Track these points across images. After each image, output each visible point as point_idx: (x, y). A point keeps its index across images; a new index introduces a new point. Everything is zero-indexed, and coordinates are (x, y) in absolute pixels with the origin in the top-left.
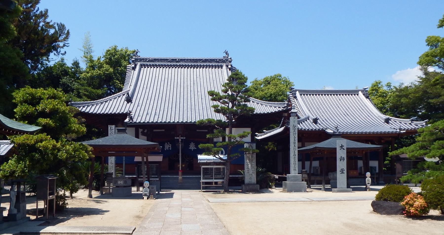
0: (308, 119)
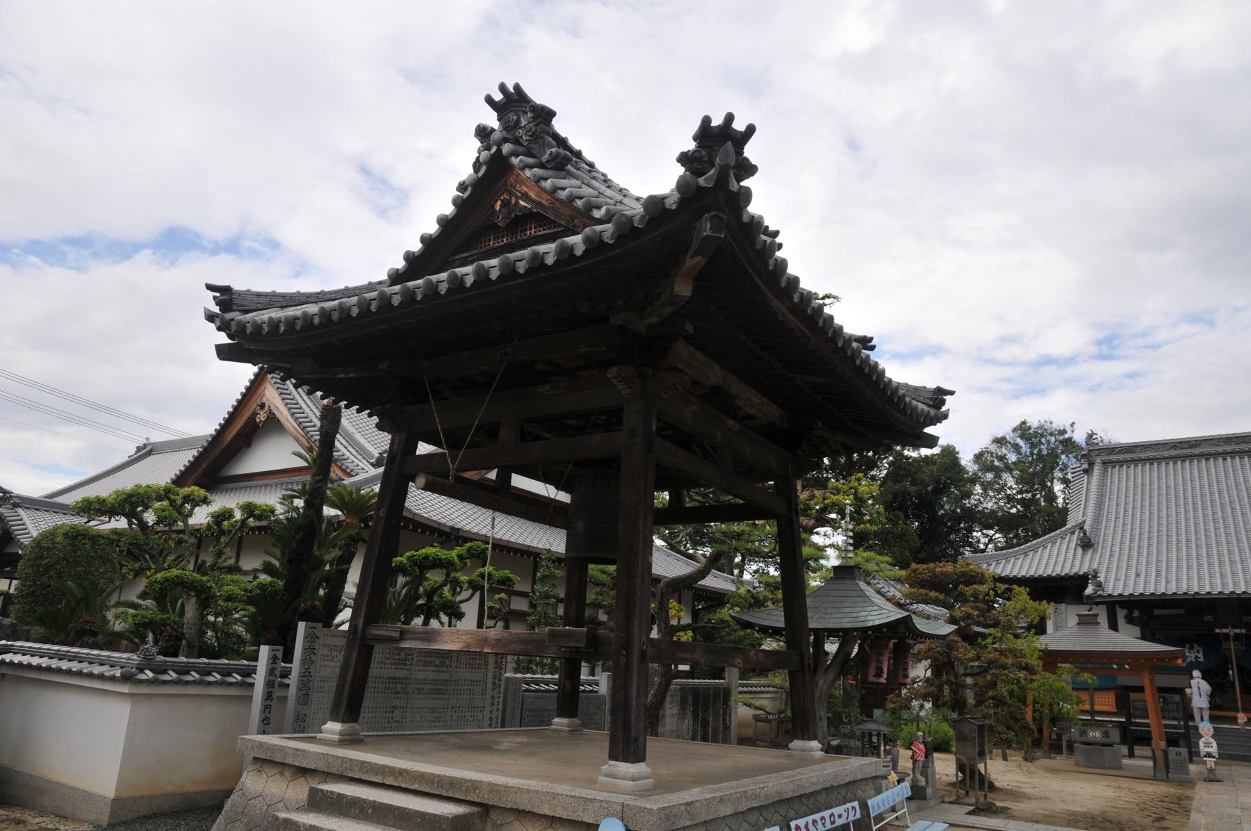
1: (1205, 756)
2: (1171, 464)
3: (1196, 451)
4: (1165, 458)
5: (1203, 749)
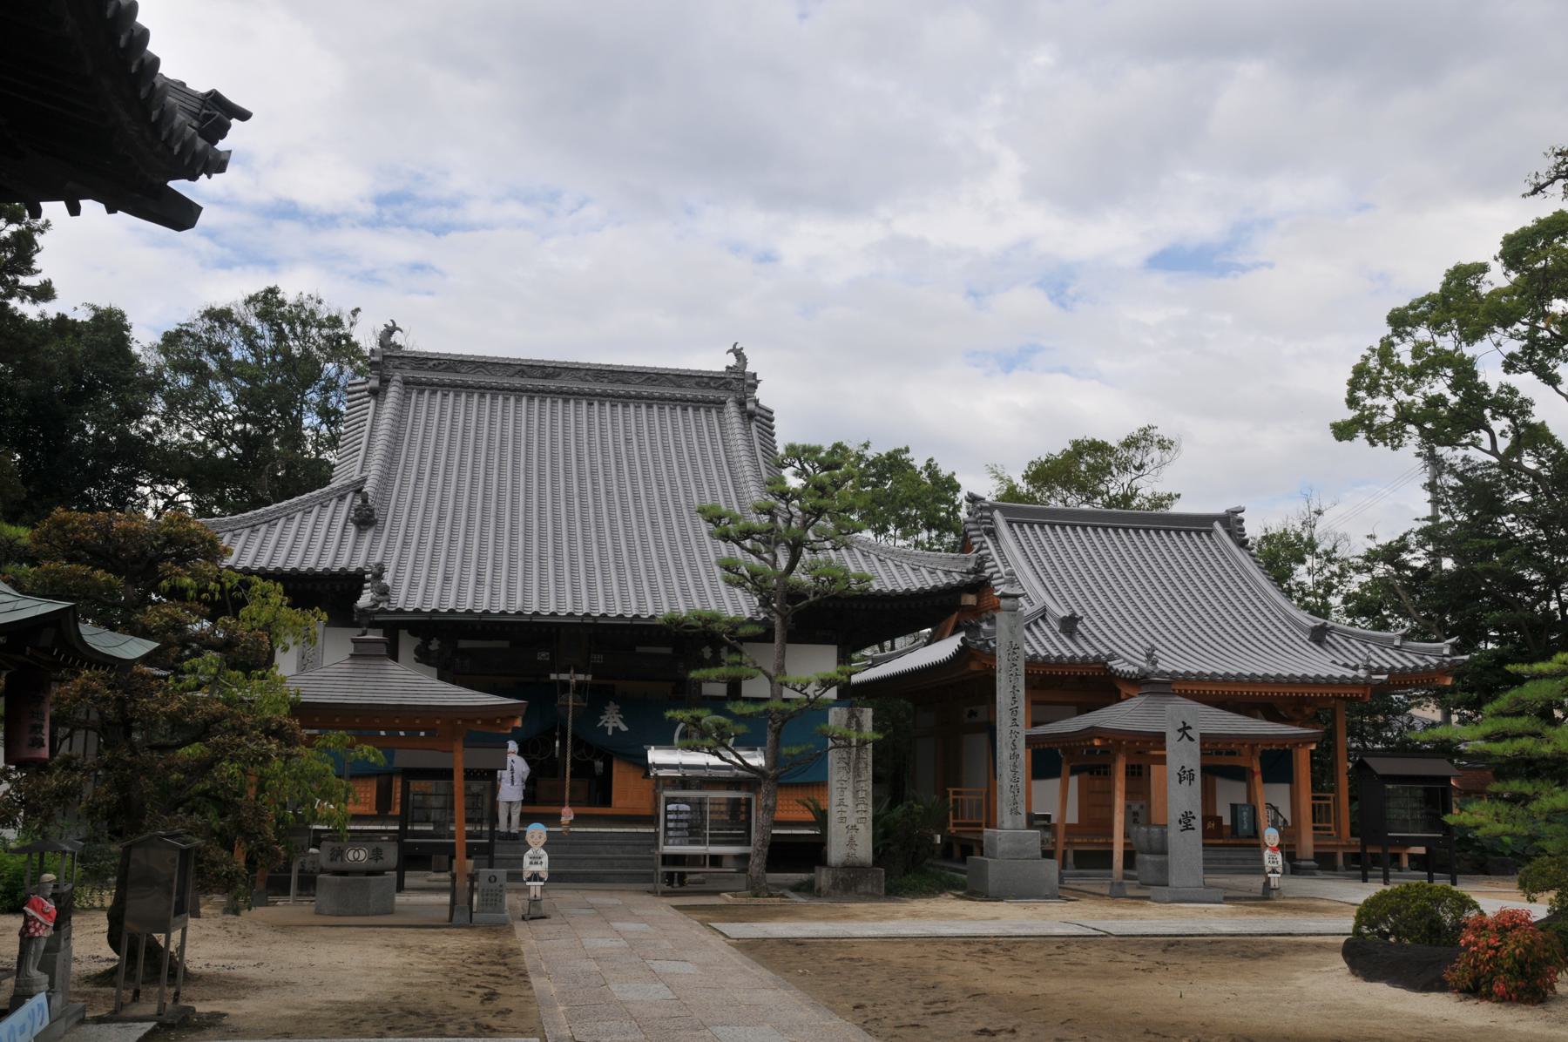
0: (1043, 618)
1: (529, 880)
2: (512, 399)
3: (552, 384)
4: (504, 389)
5: (528, 867)
